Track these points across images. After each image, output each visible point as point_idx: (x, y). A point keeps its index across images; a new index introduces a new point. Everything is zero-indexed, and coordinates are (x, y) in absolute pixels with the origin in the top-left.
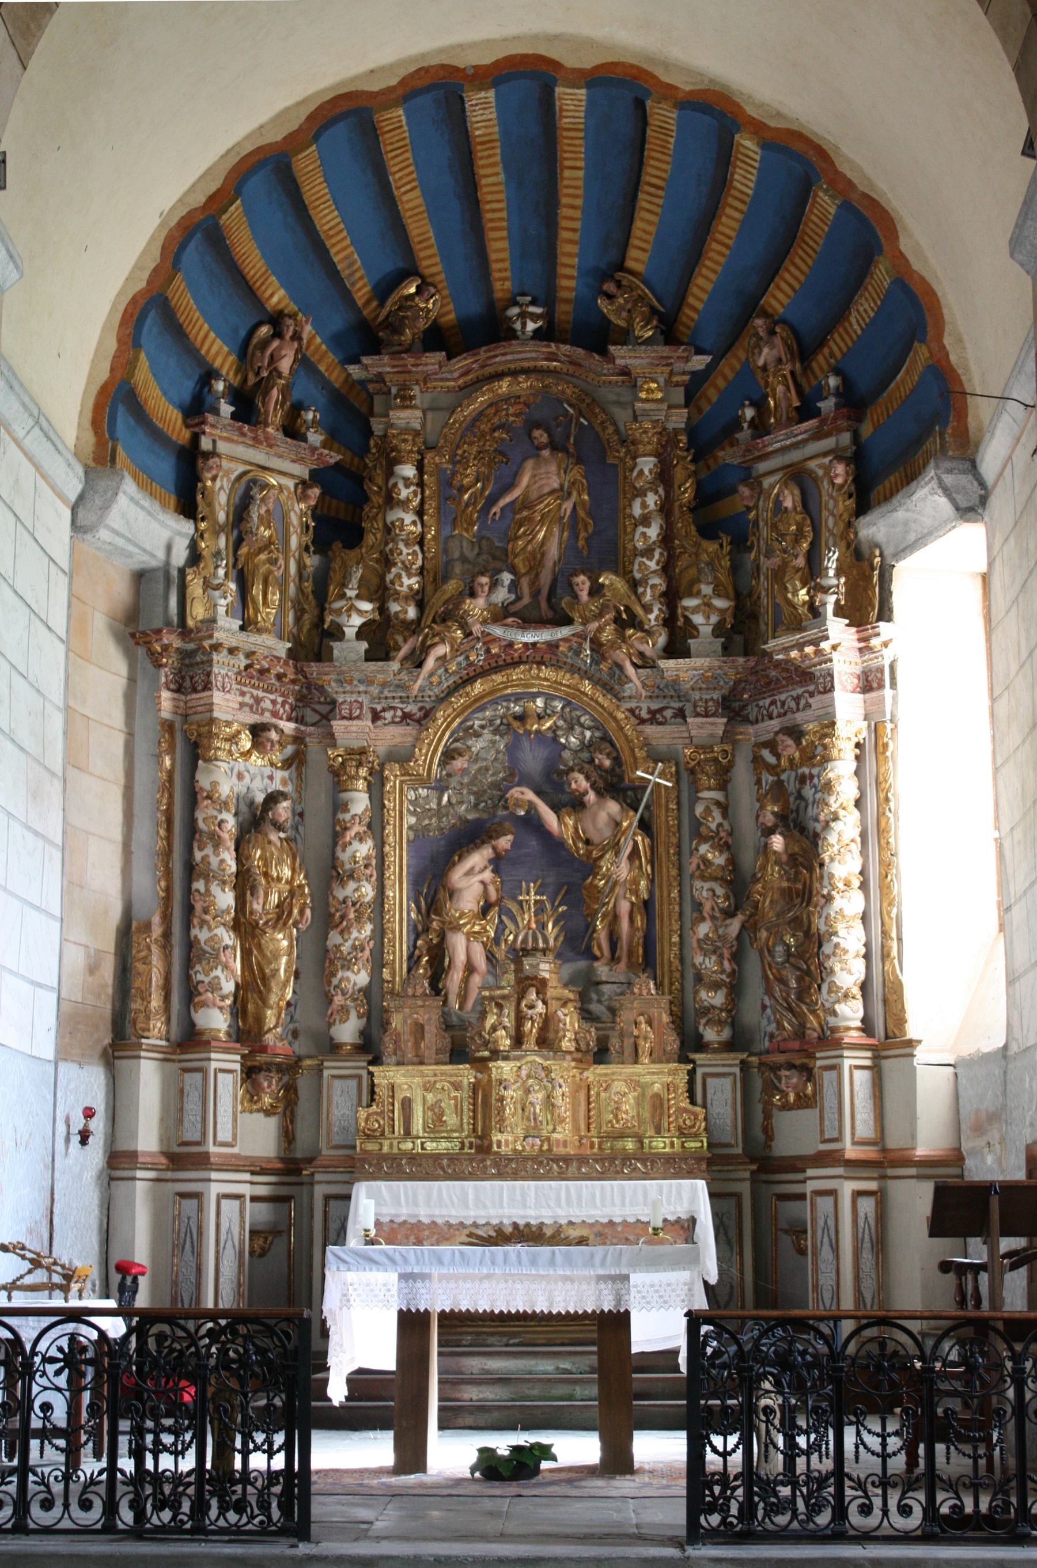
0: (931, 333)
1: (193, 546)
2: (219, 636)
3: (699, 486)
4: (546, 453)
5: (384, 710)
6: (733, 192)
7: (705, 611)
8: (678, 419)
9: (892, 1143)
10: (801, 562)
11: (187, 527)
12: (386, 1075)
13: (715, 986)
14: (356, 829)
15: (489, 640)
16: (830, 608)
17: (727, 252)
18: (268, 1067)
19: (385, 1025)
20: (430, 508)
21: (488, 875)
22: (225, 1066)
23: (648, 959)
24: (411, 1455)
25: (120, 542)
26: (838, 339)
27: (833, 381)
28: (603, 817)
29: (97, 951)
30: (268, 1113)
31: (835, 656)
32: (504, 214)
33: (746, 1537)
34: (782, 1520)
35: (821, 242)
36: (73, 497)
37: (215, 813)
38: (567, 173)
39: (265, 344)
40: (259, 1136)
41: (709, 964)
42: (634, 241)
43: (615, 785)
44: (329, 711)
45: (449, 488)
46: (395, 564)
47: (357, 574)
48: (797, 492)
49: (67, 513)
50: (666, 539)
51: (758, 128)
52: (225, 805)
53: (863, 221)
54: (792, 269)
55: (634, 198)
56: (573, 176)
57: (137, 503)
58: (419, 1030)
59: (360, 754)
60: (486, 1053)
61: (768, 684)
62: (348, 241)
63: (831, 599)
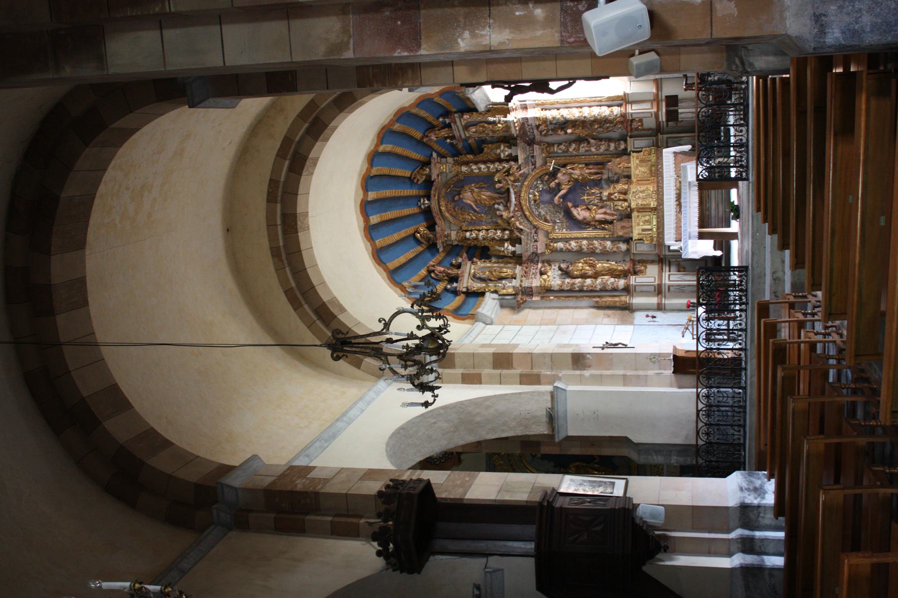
1: (493, 292)
2: (518, 285)
3: (468, 153)
7: (505, 151)
8: (450, 160)
9: (652, 98)
10: (491, 126)
11: (488, 294)
12: (635, 236)
13: (609, 146)
14: (567, 246)
15: (515, 211)
18: (634, 268)
19: (621, 236)
20: (478, 228)
21: (579, 209)
22: (634, 280)
23: (602, 164)
24: (734, 236)
27: (441, 120)
28: (562, 178)
30: (646, 268)
33: (747, 167)
39: (436, 275)
40: (652, 270)
41: (603, 148)
43: (553, 175)
44: (535, 254)
45: (472, 223)
47: (497, 247)
50: (484, 162)
51: (377, 146)
52: (563, 282)
53: (400, 118)
58: (623, 227)
59: (547, 246)
63: (502, 119)
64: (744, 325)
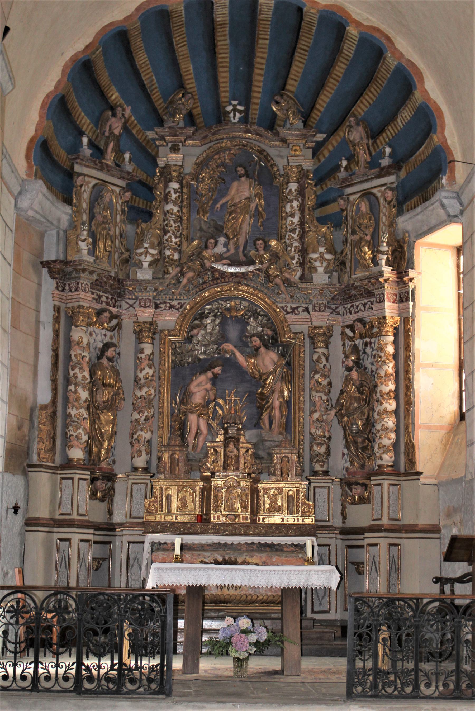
0: (439, 129)
4: (243, 179)
5: (161, 303)
6: (343, 55)
11: (68, 209)
12: (160, 483)
15: (214, 270)
16: (384, 262)
17: (338, 84)
21: (209, 386)
25: (38, 216)
26: (391, 130)
29: (22, 418)
31: (386, 285)
32: (227, 60)
34: (390, 690)
35: (386, 82)
36: (16, 193)
37: (80, 352)
38: (260, 41)
42: (291, 76)
46: (169, 232)
48: (367, 203)
49: (13, 201)
50: (302, 223)
54: (369, 94)
55: (293, 54)
56: (264, 43)
57: (46, 197)
60: (209, 474)
61: (351, 297)
62: (151, 70)
64: (48, 685)
